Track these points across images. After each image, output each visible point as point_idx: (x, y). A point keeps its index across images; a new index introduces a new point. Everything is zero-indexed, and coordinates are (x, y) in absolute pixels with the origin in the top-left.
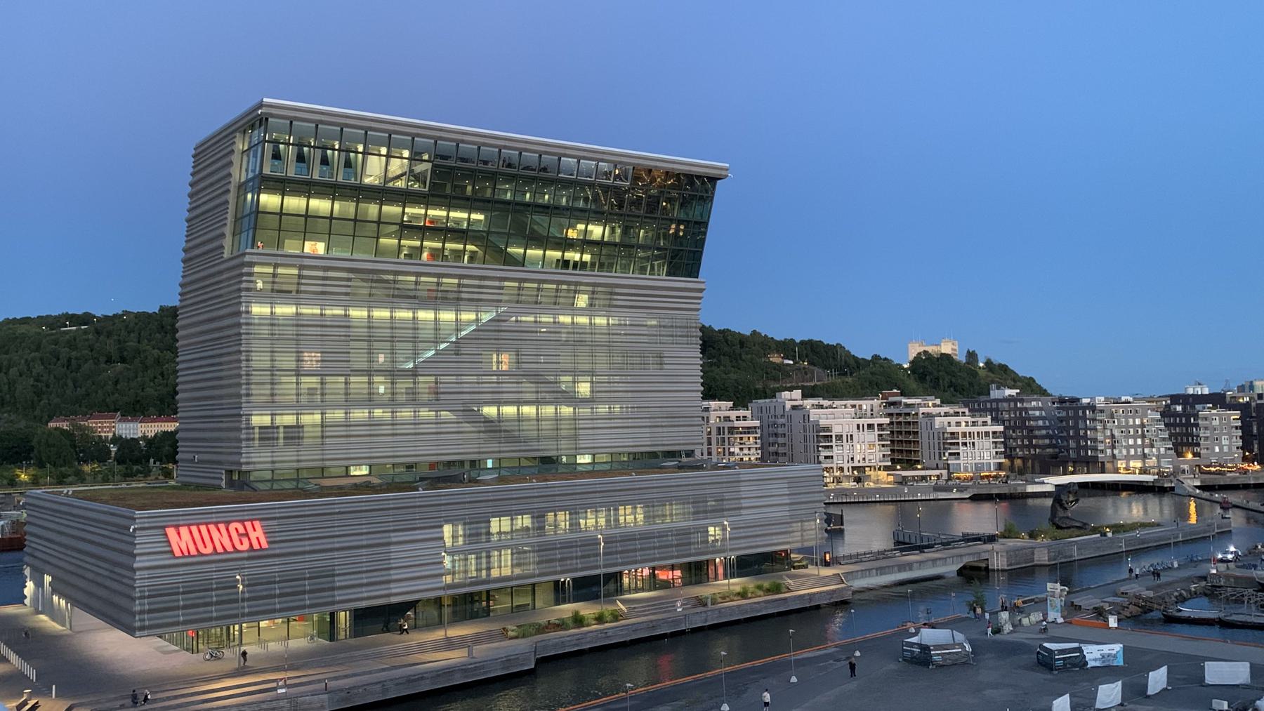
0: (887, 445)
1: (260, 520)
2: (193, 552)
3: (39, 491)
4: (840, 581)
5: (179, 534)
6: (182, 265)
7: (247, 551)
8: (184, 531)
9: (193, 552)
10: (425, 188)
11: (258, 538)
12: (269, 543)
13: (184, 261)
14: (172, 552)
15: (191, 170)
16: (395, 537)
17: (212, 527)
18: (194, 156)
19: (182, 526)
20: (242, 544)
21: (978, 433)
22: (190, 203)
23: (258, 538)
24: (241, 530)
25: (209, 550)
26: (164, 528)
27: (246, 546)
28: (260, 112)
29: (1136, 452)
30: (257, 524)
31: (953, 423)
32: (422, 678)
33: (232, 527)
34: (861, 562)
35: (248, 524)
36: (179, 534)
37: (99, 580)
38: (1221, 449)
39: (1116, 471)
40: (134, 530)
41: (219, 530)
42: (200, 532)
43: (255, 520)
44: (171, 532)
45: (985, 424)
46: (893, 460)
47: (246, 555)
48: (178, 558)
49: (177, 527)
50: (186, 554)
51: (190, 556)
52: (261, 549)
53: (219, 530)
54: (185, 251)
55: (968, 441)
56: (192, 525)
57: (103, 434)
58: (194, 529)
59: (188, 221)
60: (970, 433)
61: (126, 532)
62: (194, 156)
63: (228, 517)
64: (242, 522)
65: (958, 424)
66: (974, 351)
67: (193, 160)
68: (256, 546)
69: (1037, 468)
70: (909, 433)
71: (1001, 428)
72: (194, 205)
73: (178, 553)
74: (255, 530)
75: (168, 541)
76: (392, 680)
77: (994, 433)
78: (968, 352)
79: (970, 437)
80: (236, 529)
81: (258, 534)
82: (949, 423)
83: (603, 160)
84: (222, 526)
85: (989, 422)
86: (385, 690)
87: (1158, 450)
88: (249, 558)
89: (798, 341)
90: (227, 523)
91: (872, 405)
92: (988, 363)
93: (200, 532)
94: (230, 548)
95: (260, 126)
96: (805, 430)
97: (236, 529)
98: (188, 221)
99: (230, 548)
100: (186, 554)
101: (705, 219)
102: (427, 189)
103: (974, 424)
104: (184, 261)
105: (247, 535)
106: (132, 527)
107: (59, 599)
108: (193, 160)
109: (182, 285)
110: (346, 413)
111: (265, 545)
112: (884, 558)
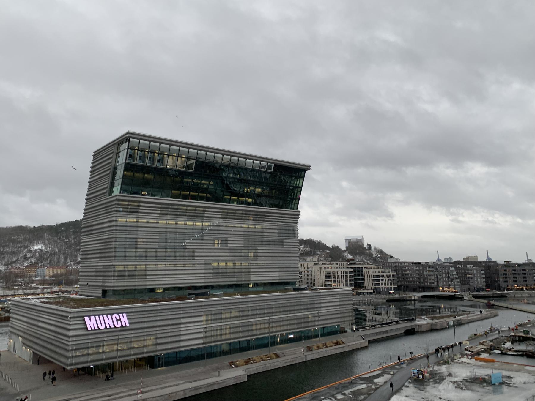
0: (352, 280)
1: (126, 313)
2: (96, 328)
3: (3, 299)
4: (362, 339)
5: (90, 319)
6: (85, 201)
7: (120, 327)
8: (92, 318)
9: (96, 328)
10: (192, 170)
11: (125, 321)
12: (129, 323)
13: (86, 199)
14: (87, 328)
15: (92, 161)
16: (183, 321)
17: (105, 316)
18: (93, 156)
19: (92, 316)
20: (118, 324)
21: (387, 275)
22: (90, 175)
23: (125, 321)
24: (118, 318)
25: (103, 327)
26: (84, 317)
27: (119, 325)
28: (127, 136)
29: (446, 283)
30: (125, 315)
31: (377, 271)
32: (201, 388)
33: (114, 316)
34: (367, 330)
35: (121, 315)
36: (90, 319)
37: (49, 340)
38: (478, 282)
39: (439, 291)
40: (70, 318)
41: (108, 318)
42: (99, 318)
43: (124, 313)
44: (87, 319)
45: (389, 272)
46: (355, 286)
47: (119, 329)
48: (89, 331)
49: (89, 316)
50: (93, 329)
51: (95, 330)
52: (126, 326)
53: (108, 318)
54: (87, 195)
55: (383, 278)
56: (100, 315)
57: (31, 274)
58: (97, 317)
59: (89, 182)
60: (384, 275)
61: (66, 319)
62: (93, 156)
63: (112, 312)
64: (118, 314)
65: (379, 272)
66: (370, 244)
67: (93, 157)
68: (124, 325)
69: (423, 291)
70: (359, 275)
71: (395, 274)
72: (93, 176)
73: (89, 329)
74: (124, 318)
75: (85, 323)
76: (188, 389)
77: (393, 275)
78: (368, 244)
79: (384, 277)
80: (116, 317)
81: (125, 320)
82: (375, 271)
83: (263, 161)
84: (109, 316)
85: (391, 271)
86: (185, 394)
87: (454, 283)
88: (120, 331)
89: (305, 239)
90: (112, 315)
91: (344, 264)
92: (375, 248)
93: (99, 318)
94: (112, 326)
95: (126, 142)
96: (320, 274)
97: (116, 317)
98: (89, 182)
99: (112, 326)
100: (93, 329)
101: (300, 186)
102: (193, 171)
103: (385, 272)
104: (86, 199)
105: (120, 320)
106: (69, 317)
107: (26, 348)
108: (93, 157)
109: (85, 210)
110: (234, 264)
111: (128, 325)
112: (375, 328)
